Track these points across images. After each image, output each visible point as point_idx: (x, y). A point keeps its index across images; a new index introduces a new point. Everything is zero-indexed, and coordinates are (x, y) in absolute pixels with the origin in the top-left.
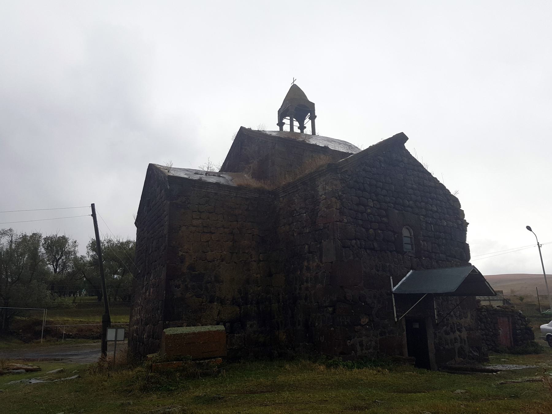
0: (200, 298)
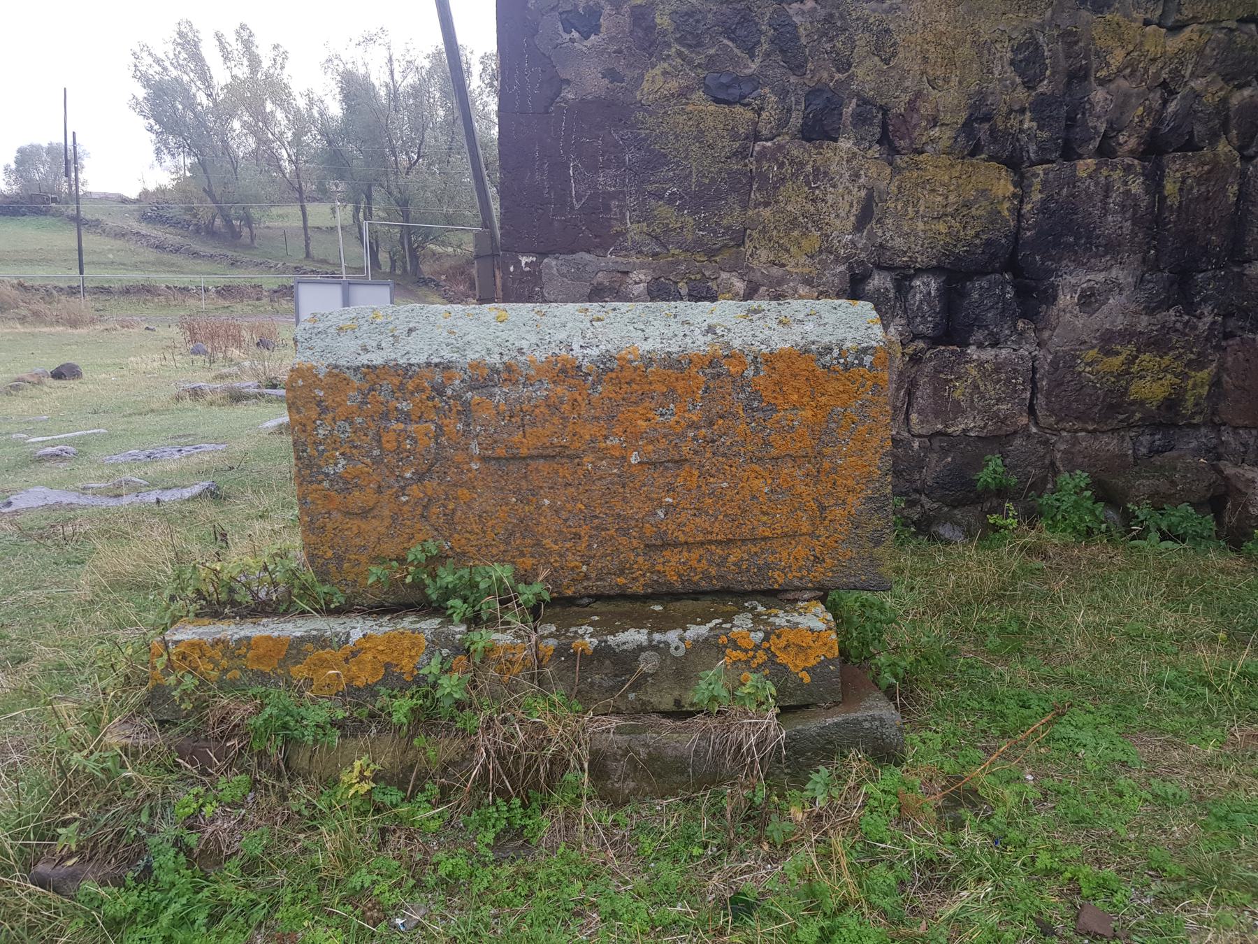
0: (738, 109)
